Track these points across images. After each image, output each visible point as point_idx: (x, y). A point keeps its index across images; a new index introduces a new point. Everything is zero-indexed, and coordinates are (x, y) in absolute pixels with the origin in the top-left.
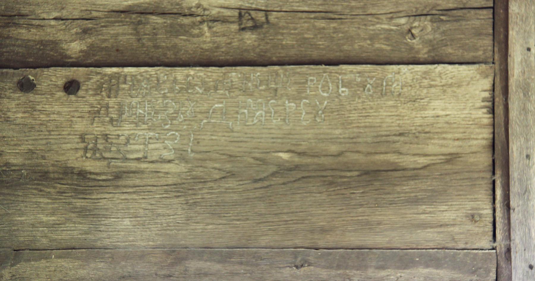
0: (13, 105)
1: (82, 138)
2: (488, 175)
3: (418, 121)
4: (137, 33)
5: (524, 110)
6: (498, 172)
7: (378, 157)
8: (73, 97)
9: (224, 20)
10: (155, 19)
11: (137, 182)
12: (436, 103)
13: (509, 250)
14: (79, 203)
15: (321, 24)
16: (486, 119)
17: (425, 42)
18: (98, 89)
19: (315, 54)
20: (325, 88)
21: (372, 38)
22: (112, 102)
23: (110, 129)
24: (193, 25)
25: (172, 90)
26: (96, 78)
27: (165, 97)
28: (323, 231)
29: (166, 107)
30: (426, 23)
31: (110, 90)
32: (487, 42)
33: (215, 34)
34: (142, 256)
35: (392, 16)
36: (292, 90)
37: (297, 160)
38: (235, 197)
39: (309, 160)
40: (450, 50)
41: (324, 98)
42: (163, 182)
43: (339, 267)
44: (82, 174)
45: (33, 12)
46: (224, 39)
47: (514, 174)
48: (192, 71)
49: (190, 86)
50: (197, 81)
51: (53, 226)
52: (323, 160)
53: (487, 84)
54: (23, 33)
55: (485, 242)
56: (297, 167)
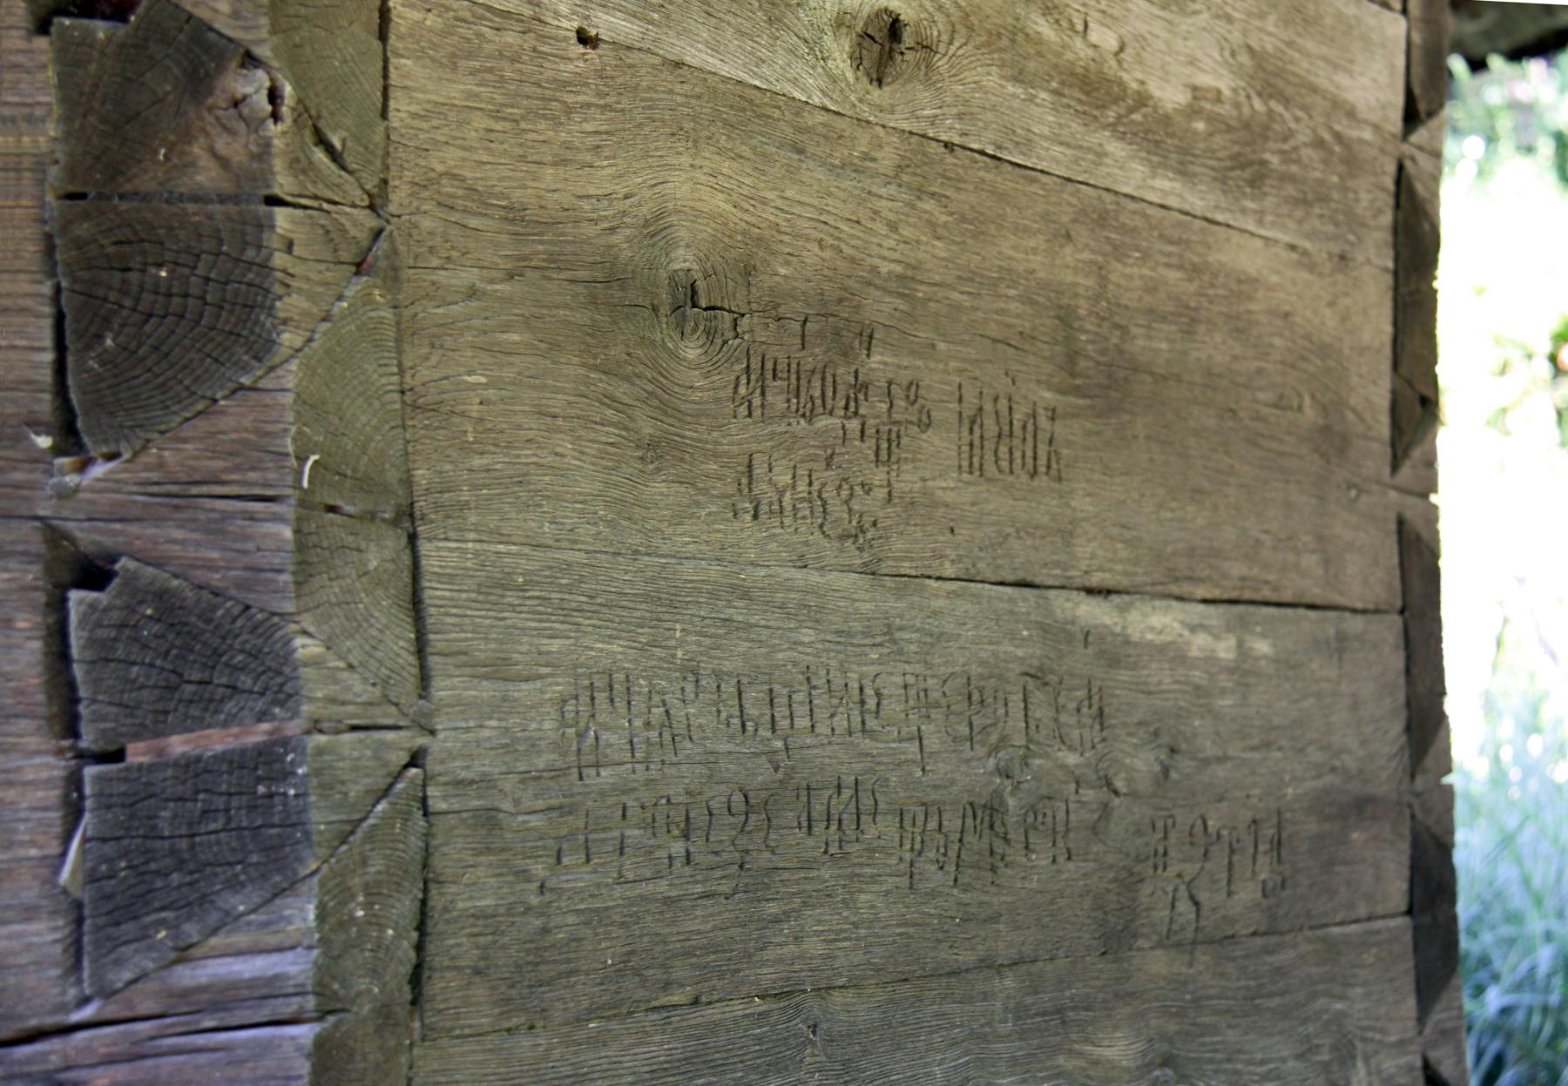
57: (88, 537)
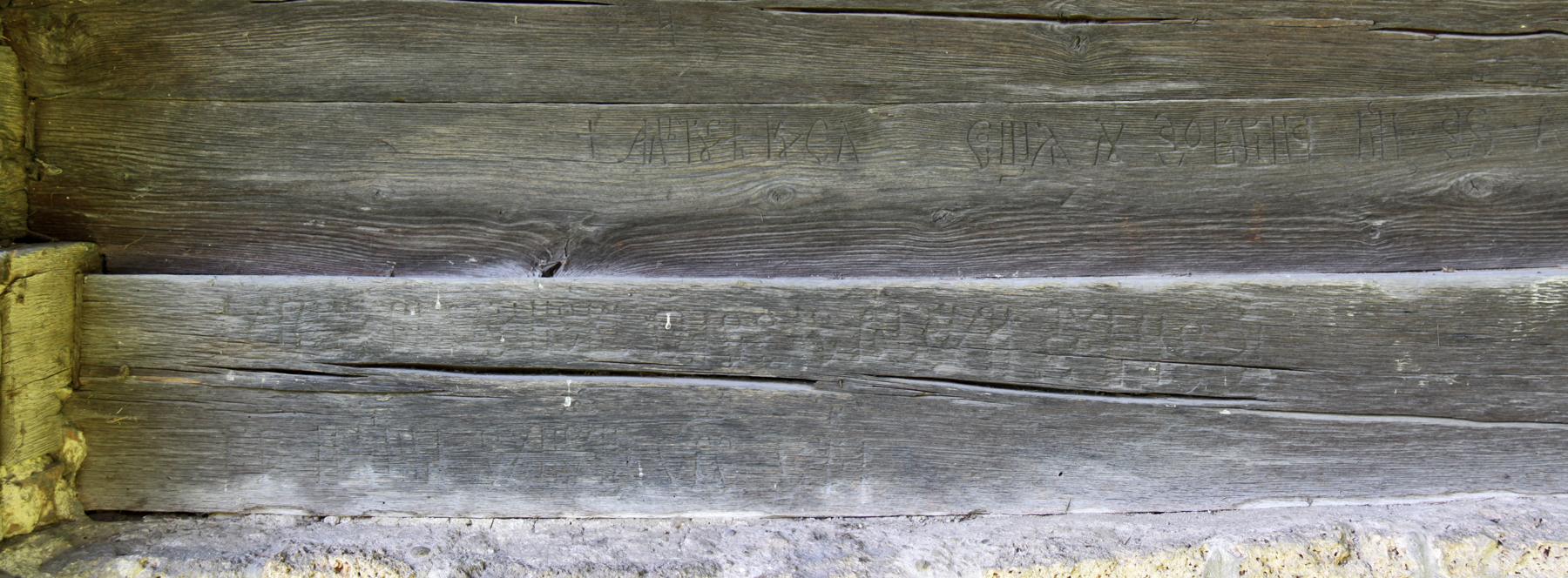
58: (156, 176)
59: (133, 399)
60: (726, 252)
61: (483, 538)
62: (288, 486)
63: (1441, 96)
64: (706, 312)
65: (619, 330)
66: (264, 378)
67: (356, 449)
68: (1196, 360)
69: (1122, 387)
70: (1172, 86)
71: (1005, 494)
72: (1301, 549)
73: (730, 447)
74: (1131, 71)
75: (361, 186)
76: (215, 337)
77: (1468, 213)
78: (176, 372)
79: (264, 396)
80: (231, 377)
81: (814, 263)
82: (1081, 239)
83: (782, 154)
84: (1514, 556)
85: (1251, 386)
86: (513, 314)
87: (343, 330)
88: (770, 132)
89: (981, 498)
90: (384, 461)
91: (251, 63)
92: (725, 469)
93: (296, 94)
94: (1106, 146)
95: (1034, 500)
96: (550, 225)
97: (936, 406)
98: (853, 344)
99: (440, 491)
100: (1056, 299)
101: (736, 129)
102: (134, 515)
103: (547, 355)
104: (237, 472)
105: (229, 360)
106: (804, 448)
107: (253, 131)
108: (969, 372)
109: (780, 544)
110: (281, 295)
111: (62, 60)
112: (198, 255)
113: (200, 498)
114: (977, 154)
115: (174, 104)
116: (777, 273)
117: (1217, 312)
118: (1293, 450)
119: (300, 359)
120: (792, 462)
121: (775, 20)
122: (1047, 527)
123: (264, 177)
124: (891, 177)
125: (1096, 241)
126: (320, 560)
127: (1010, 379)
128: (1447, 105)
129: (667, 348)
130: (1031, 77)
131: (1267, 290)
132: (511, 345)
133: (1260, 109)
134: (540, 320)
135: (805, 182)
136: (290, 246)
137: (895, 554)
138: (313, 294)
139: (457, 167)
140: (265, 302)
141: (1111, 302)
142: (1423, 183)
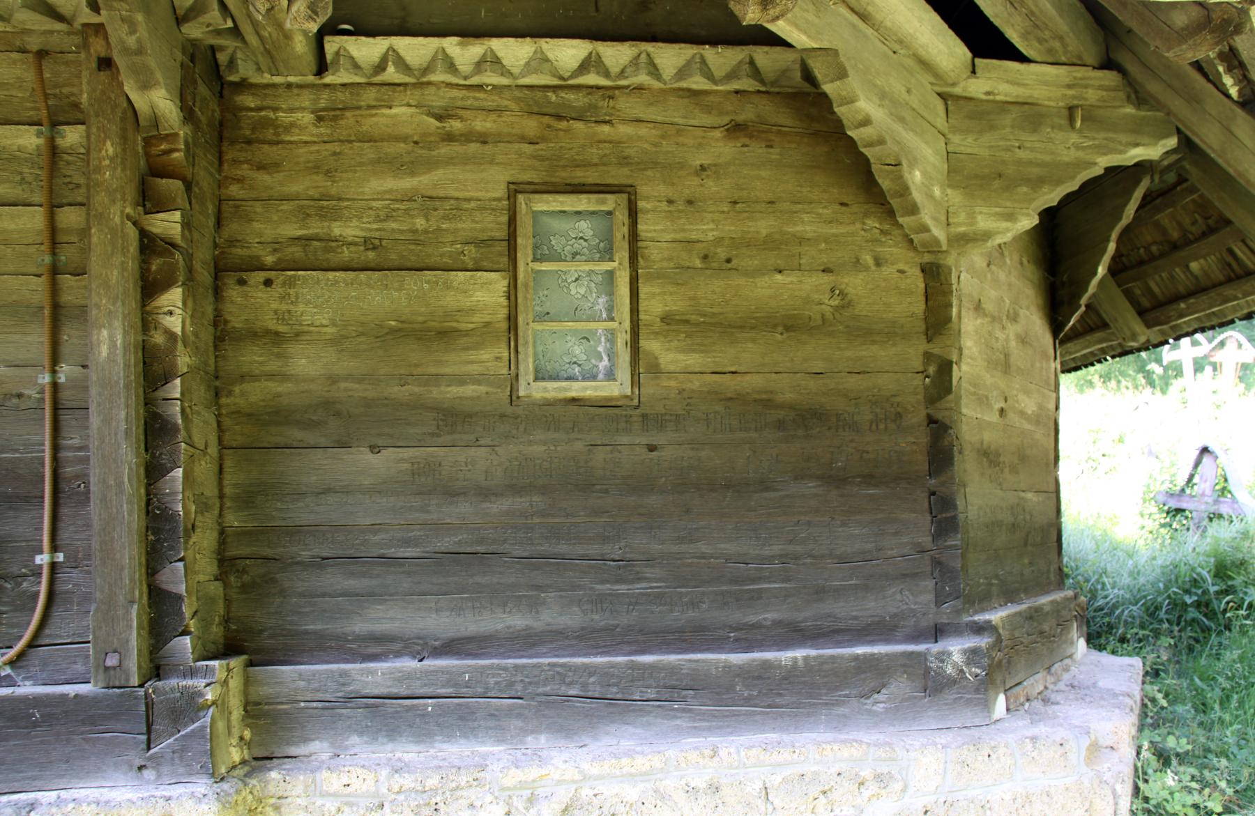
0: (235, 293)
1: (276, 312)
2: (507, 334)
3: (468, 304)
4: (305, 251)
5: (526, 298)
6: (512, 333)
7: (446, 324)
8: (269, 289)
9: (356, 244)
10: (315, 243)
11: (308, 338)
12: (478, 294)
13: (517, 375)
14: (276, 350)
15: (412, 247)
16: (505, 303)
17: (472, 259)
18: (284, 284)
19: (409, 265)
20: (415, 284)
21: (441, 255)
22: (292, 291)
23: (292, 307)
24: (338, 247)
25: (326, 284)
26: (282, 278)
27: (322, 288)
28: (416, 365)
29: (323, 295)
30: (472, 247)
31: (290, 284)
32: (505, 259)
33: (351, 252)
34: (313, 380)
35: (453, 243)
36: (396, 285)
37: (400, 325)
38: (365, 346)
39: (406, 326)
40: (485, 264)
41: (414, 290)
42: (323, 338)
43: (425, 386)
44: (277, 333)
45: (244, 239)
46: (356, 255)
47: (520, 333)
48: (338, 274)
49: (337, 282)
50: (340, 279)
51: (262, 363)
52: (415, 326)
53: (505, 283)
54: (239, 251)
55: (505, 371)
56: (400, 330)
57: (932, 489)
58: (271, 628)
59: (266, 714)
60: (490, 650)
61: (399, 760)
62: (326, 745)
63: (751, 587)
64: (481, 673)
65: (449, 681)
66: (315, 704)
67: (351, 730)
68: (666, 687)
69: (638, 698)
70: (655, 584)
71: (595, 738)
72: (698, 752)
73: (492, 723)
74: (640, 579)
75: (348, 629)
76: (296, 689)
77: (763, 630)
78: (282, 703)
79: (316, 711)
80: (303, 704)
81: (521, 653)
82: (623, 642)
83: (510, 612)
84: (769, 753)
85: (685, 697)
86: (409, 676)
87: (343, 685)
88: (505, 604)
89: (585, 739)
90: (361, 734)
91: (307, 584)
92: (490, 732)
93: (324, 595)
94: (631, 607)
95: (606, 740)
96: (421, 642)
97: (569, 706)
98: (537, 684)
99: (383, 744)
100: (613, 665)
101: (492, 604)
102: (271, 758)
103: (422, 691)
104: (306, 740)
105: (302, 698)
106: (520, 723)
107: (307, 610)
108: (582, 694)
109: (510, 757)
110: (320, 672)
111: (239, 585)
112: (286, 658)
113: (293, 751)
114: (583, 611)
115: (278, 600)
116: (509, 657)
117: (673, 670)
118: (700, 720)
119: (328, 697)
120: (515, 729)
121: (506, 562)
122: (610, 749)
123: (311, 627)
124: (550, 620)
125: (629, 643)
126: (342, 769)
127: (597, 696)
128: (753, 590)
129: (467, 687)
130: (603, 582)
131: (690, 661)
132: (408, 688)
133: (688, 593)
134: (418, 678)
135: (519, 622)
136: (322, 653)
137: (552, 759)
138: (332, 671)
139: (384, 621)
140: (314, 675)
141: (633, 666)
142: (747, 619)
